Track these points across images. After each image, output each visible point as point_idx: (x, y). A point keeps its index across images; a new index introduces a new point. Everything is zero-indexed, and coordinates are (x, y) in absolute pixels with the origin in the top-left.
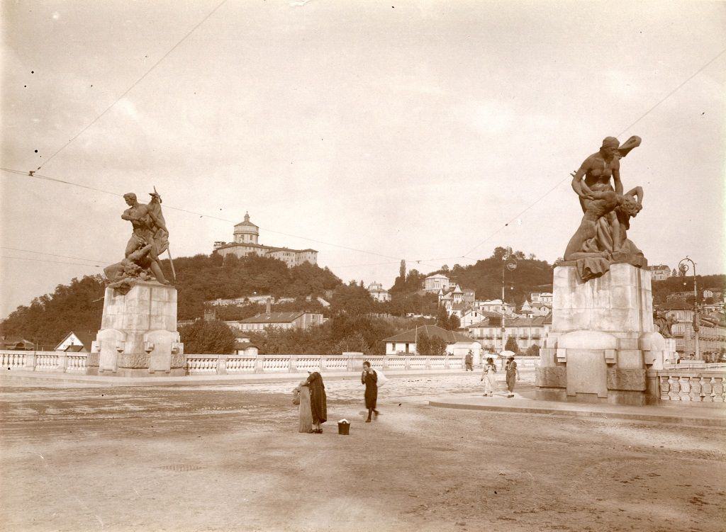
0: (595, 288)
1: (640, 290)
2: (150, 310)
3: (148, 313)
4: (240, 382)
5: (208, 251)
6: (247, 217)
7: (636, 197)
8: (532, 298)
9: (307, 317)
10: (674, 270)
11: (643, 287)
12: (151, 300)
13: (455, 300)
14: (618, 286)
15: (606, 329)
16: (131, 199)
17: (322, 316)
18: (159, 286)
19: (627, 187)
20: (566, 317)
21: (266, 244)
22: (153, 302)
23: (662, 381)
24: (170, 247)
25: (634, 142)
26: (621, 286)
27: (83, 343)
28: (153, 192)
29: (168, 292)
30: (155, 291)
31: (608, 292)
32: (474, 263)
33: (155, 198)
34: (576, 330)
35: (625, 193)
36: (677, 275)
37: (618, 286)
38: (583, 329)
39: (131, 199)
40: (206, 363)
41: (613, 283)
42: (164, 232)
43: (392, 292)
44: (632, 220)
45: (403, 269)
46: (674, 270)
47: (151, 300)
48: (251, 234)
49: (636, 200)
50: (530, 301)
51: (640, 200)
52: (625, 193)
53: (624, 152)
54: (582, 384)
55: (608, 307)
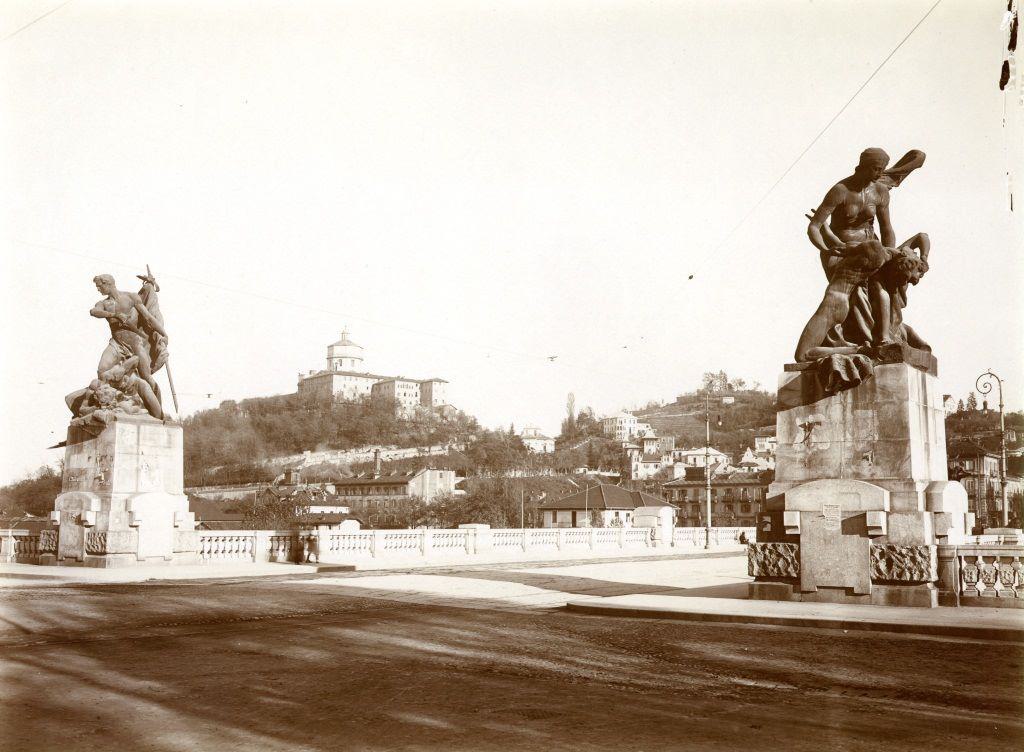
0: (849, 406)
1: (926, 409)
4: (573, 563)
5: (292, 389)
7: (917, 250)
8: (757, 445)
10: (961, 401)
11: (930, 404)
12: (138, 444)
13: (647, 448)
16: (103, 284)
18: (153, 422)
19: (901, 235)
20: (800, 456)
23: (964, 564)
24: (171, 361)
25: (913, 160)
28: (144, 273)
32: (674, 400)
34: (816, 479)
35: (899, 242)
36: (965, 409)
39: (103, 284)
40: (228, 545)
41: (879, 399)
42: (160, 337)
44: (910, 289)
45: (570, 406)
46: (961, 401)
47: (138, 444)
49: (919, 255)
50: (753, 449)
52: (899, 242)
53: (898, 175)
54: (827, 571)
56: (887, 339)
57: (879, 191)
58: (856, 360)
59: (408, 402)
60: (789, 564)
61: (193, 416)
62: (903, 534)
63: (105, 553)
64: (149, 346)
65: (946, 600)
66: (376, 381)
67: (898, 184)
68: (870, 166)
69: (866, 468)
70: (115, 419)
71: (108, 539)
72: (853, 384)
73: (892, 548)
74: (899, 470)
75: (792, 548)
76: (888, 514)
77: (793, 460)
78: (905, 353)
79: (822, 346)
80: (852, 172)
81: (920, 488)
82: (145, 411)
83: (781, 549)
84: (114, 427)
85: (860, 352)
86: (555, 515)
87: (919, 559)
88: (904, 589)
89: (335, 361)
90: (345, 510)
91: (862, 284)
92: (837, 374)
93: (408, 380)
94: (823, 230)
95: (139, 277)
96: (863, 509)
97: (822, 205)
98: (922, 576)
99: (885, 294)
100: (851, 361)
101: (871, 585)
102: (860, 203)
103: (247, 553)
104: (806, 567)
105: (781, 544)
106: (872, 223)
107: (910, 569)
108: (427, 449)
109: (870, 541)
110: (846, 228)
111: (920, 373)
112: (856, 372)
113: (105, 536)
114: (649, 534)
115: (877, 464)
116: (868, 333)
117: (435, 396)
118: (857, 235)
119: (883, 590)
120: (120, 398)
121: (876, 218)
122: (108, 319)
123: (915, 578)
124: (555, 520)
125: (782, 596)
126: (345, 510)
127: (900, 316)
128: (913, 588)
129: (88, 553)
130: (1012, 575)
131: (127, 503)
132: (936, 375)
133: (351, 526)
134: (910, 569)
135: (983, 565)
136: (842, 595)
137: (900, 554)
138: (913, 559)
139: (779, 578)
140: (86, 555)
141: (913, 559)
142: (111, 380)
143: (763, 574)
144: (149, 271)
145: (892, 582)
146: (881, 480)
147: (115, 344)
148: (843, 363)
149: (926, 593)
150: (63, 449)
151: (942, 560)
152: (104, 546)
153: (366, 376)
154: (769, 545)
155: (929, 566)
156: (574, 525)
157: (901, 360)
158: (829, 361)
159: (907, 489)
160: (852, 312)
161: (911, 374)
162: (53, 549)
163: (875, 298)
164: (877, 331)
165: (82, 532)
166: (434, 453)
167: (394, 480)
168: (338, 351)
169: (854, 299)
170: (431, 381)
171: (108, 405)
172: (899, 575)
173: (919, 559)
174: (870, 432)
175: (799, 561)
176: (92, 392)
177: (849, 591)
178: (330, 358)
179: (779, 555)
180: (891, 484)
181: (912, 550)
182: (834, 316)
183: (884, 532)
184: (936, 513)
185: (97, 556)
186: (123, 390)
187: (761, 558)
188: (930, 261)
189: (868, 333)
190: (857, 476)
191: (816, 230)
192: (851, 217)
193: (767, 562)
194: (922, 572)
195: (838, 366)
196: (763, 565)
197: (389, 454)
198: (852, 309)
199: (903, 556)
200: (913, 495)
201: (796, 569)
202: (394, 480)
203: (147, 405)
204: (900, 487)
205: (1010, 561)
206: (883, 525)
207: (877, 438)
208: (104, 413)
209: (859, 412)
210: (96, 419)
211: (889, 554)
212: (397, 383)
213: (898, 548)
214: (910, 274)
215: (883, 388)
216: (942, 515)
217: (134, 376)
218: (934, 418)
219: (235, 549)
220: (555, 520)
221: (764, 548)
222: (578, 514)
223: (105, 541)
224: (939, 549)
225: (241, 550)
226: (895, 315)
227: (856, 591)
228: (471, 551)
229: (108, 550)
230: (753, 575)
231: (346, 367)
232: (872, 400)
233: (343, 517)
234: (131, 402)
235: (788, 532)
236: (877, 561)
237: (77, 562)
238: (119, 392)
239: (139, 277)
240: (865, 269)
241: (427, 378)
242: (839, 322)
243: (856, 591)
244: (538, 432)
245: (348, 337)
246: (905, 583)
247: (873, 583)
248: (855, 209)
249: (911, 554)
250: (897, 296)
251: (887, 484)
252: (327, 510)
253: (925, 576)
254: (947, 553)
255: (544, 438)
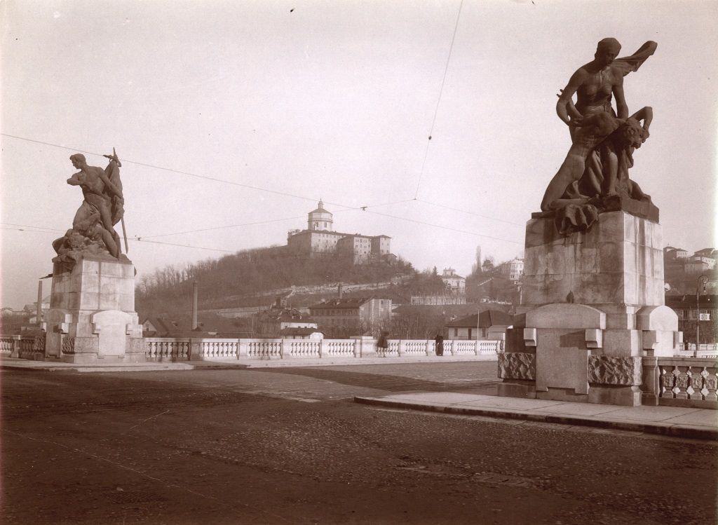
1: (643, 248)
2: (99, 287)
3: (97, 291)
5: (283, 241)
6: (320, 204)
9: (376, 304)
11: (648, 244)
14: (609, 243)
15: (591, 302)
16: (78, 160)
17: (390, 301)
19: (633, 108)
21: (339, 231)
22: (102, 279)
23: (665, 372)
24: (125, 216)
26: (612, 243)
27: (156, 329)
29: (123, 267)
30: (105, 265)
31: (594, 251)
33: (114, 162)
35: (630, 115)
37: (609, 243)
38: (561, 302)
39: (78, 160)
41: (602, 239)
43: (469, 281)
48: (326, 222)
49: (642, 125)
51: (647, 124)
52: (630, 115)
53: (635, 62)
55: (594, 271)
56: (612, 192)
57: (614, 73)
58: (586, 210)
59: (362, 249)
60: (527, 370)
61: (218, 261)
62: (615, 348)
63: (73, 353)
64: (111, 205)
65: (647, 400)
66: (341, 237)
67: (635, 70)
68: (607, 49)
69: (589, 295)
70: (83, 258)
71: (76, 343)
72: (582, 229)
73: (604, 358)
74: (614, 296)
75: (530, 356)
76: (604, 331)
77: (536, 289)
78: (623, 203)
79: (562, 198)
80: (593, 59)
81: (631, 312)
82: (108, 252)
83: (522, 358)
84: (81, 264)
85: (590, 203)
86: (456, 331)
87: (625, 367)
88: (613, 391)
89: (314, 223)
90: (314, 326)
91: (595, 149)
92: (568, 220)
93: (363, 237)
94: (568, 106)
95: (106, 156)
96: (584, 327)
97: (568, 86)
98: (626, 381)
99: (613, 156)
100: (581, 209)
101: (588, 387)
102: (599, 84)
103: (278, 354)
104: (539, 375)
105: (522, 354)
106: (610, 99)
107: (617, 375)
108: (375, 285)
109: (589, 352)
110: (588, 105)
111: (638, 220)
112: (584, 218)
113: (73, 340)
114: (499, 346)
115: (598, 291)
116: (598, 186)
117: (382, 248)
118: (595, 109)
119: (598, 390)
120: (87, 243)
121: (613, 96)
122: (81, 186)
123: (622, 382)
124: (456, 335)
125: (522, 394)
126: (314, 326)
127: (627, 174)
128: (620, 390)
129: (64, 352)
130: (701, 383)
131: (91, 317)
132: (657, 221)
133: (317, 337)
134: (617, 375)
135: (677, 372)
136: (564, 394)
137: (611, 363)
138: (620, 368)
139: (520, 379)
140: (62, 354)
141: (620, 368)
142: (80, 230)
143: (508, 377)
144: (115, 153)
145: (604, 385)
146: (601, 305)
147: (87, 204)
148: (574, 211)
149: (630, 394)
150: (51, 278)
151: (646, 369)
152: (73, 348)
153: (335, 233)
154: (513, 355)
155: (632, 373)
156: (470, 338)
157: (619, 209)
158: (563, 210)
159: (620, 312)
160: (587, 172)
161: (629, 221)
162: (42, 349)
163: (605, 159)
164: (606, 185)
165: (60, 337)
166: (380, 288)
167: (352, 304)
168: (315, 216)
169: (589, 161)
170: (379, 238)
171: (77, 247)
172: (610, 380)
173: (625, 367)
174: (592, 268)
175: (535, 368)
176: (67, 238)
177: (570, 391)
178: (310, 221)
179: (520, 363)
180: (608, 308)
181: (619, 360)
182: (572, 174)
183: (600, 346)
184: (643, 331)
185: (70, 352)
186: (90, 237)
187: (506, 364)
188: (651, 129)
189: (598, 186)
190: (583, 301)
191: (563, 106)
192: (590, 96)
193: (511, 368)
194: (627, 378)
195: (570, 214)
196: (508, 370)
197: (347, 288)
198: (587, 170)
199: (613, 365)
200: (624, 316)
201: (532, 373)
202: (352, 304)
203: (108, 248)
204: (613, 310)
205: (700, 370)
206: (535, 338)
207: (599, 271)
208: (75, 254)
209: (586, 251)
210: (69, 257)
211: (603, 362)
212: (355, 238)
213: (609, 359)
214: (633, 140)
215: (605, 231)
216: (649, 333)
217: (99, 226)
218: (652, 255)
219: (302, 350)
220: (456, 335)
221: (509, 357)
222: (473, 331)
223: (74, 344)
224: (644, 360)
225: (342, 350)
226: (622, 174)
227: (577, 391)
228: (358, 355)
229: (75, 351)
230: (500, 378)
231: (322, 227)
232: (596, 242)
233: (313, 330)
234: (96, 245)
235: (527, 344)
236: (593, 369)
237: (56, 358)
238: (87, 238)
239: (106, 156)
240: (597, 136)
241: (377, 234)
242: (576, 179)
243: (577, 391)
244: (454, 273)
245: (324, 207)
246: (614, 386)
247: (590, 384)
248: (594, 89)
249: (618, 363)
250: (624, 156)
251: (604, 308)
252: (303, 325)
253: (629, 381)
254: (650, 364)
255: (458, 277)
